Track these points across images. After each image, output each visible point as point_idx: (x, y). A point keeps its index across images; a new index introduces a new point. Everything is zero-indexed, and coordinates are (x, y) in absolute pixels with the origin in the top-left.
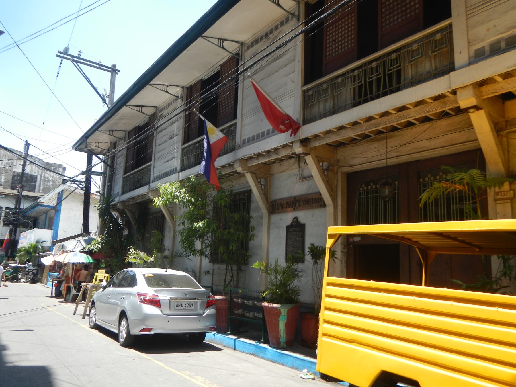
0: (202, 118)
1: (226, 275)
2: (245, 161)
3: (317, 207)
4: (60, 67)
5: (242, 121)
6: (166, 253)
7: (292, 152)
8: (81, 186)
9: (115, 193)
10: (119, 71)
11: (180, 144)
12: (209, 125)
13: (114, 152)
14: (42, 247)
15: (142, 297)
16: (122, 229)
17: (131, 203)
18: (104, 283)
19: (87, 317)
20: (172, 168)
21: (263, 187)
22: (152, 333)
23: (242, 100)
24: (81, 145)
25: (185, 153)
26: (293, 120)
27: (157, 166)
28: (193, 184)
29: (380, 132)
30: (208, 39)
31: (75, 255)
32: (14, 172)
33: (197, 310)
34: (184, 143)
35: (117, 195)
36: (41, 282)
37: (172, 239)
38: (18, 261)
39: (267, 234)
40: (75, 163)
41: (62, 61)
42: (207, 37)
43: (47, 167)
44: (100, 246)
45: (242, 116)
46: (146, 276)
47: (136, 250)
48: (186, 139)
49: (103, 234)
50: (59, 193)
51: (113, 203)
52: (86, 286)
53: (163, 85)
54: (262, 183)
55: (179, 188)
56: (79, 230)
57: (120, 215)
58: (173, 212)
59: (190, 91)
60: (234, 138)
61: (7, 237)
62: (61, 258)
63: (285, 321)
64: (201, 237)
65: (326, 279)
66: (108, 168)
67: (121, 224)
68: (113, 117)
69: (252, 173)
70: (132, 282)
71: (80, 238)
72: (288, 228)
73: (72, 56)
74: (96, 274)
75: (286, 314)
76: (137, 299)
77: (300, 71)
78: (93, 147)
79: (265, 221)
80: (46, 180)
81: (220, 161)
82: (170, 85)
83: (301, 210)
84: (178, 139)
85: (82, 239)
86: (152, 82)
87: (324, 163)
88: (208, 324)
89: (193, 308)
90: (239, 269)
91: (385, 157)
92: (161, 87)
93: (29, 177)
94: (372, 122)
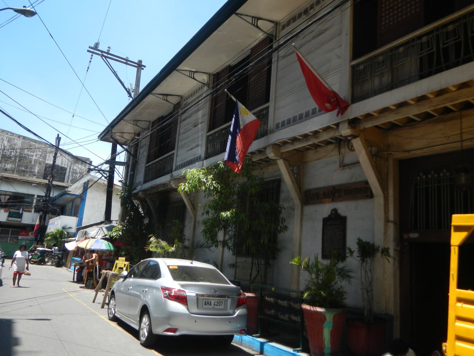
0: (234, 99)
1: (252, 269)
2: (277, 146)
3: (362, 198)
4: (90, 62)
5: (275, 104)
6: (187, 243)
7: (340, 134)
8: (105, 175)
9: (137, 182)
10: (145, 67)
11: (205, 131)
12: (241, 107)
13: (138, 139)
14: (68, 233)
15: (167, 292)
16: (143, 217)
17: (152, 192)
18: (125, 273)
19: (106, 306)
20: (196, 156)
21: (296, 175)
22: (177, 334)
23: (276, 82)
24: (106, 135)
25: (210, 140)
26: (340, 98)
27: (181, 154)
28: (220, 171)
29: (447, 111)
30: (242, 17)
31: (97, 241)
32: (46, 164)
33: (227, 310)
34: (209, 130)
35: (139, 184)
36: (65, 266)
37: (194, 227)
38: (46, 245)
39: (299, 226)
40: (100, 153)
41: (92, 56)
42: (241, 15)
43: (77, 159)
44: (121, 233)
45: (275, 99)
46: (171, 267)
47: (157, 238)
48: (211, 127)
49: (124, 222)
50: (85, 183)
51: (135, 191)
52: (107, 273)
53: (190, 71)
54: (295, 171)
55: (206, 174)
56: (102, 218)
57: (141, 203)
58: (194, 201)
59: (216, 78)
60: (266, 123)
61: (37, 223)
62: (83, 245)
63: (331, 329)
64: (225, 227)
65: (454, 292)
66: (131, 157)
67: (142, 212)
68: (139, 105)
69: (285, 160)
70: (154, 273)
71: (102, 225)
72: (326, 221)
73: (102, 52)
74: (117, 261)
75: (331, 321)
76: (161, 294)
77: (348, 45)
78: (118, 137)
79: (297, 212)
80: (75, 172)
81: (255, 146)
82: (197, 72)
83: (341, 201)
84: (203, 127)
85: (104, 226)
86: (180, 67)
87: (373, 149)
88: (239, 325)
89: (222, 307)
90: (267, 264)
91: (459, 139)
92: (188, 73)
93: (59, 169)
94: (446, 96)
